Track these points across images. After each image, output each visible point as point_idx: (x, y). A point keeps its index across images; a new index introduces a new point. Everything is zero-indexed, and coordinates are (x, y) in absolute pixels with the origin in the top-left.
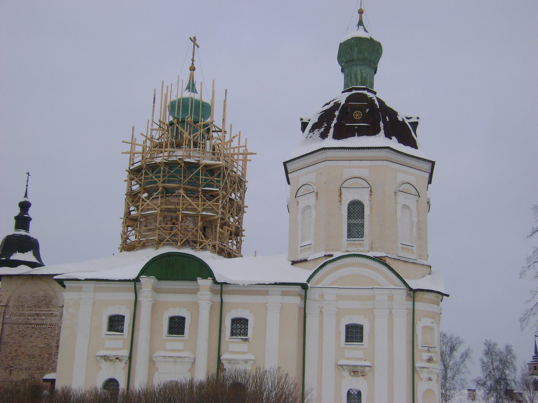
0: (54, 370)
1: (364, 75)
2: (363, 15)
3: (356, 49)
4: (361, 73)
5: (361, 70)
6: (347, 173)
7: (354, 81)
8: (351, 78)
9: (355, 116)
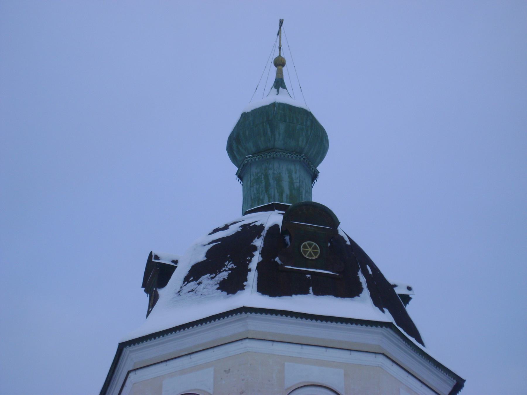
1: (297, 185)
2: (284, 69)
3: (282, 127)
4: (290, 177)
5: (290, 172)
7: (273, 191)
8: (267, 187)
9: (305, 252)
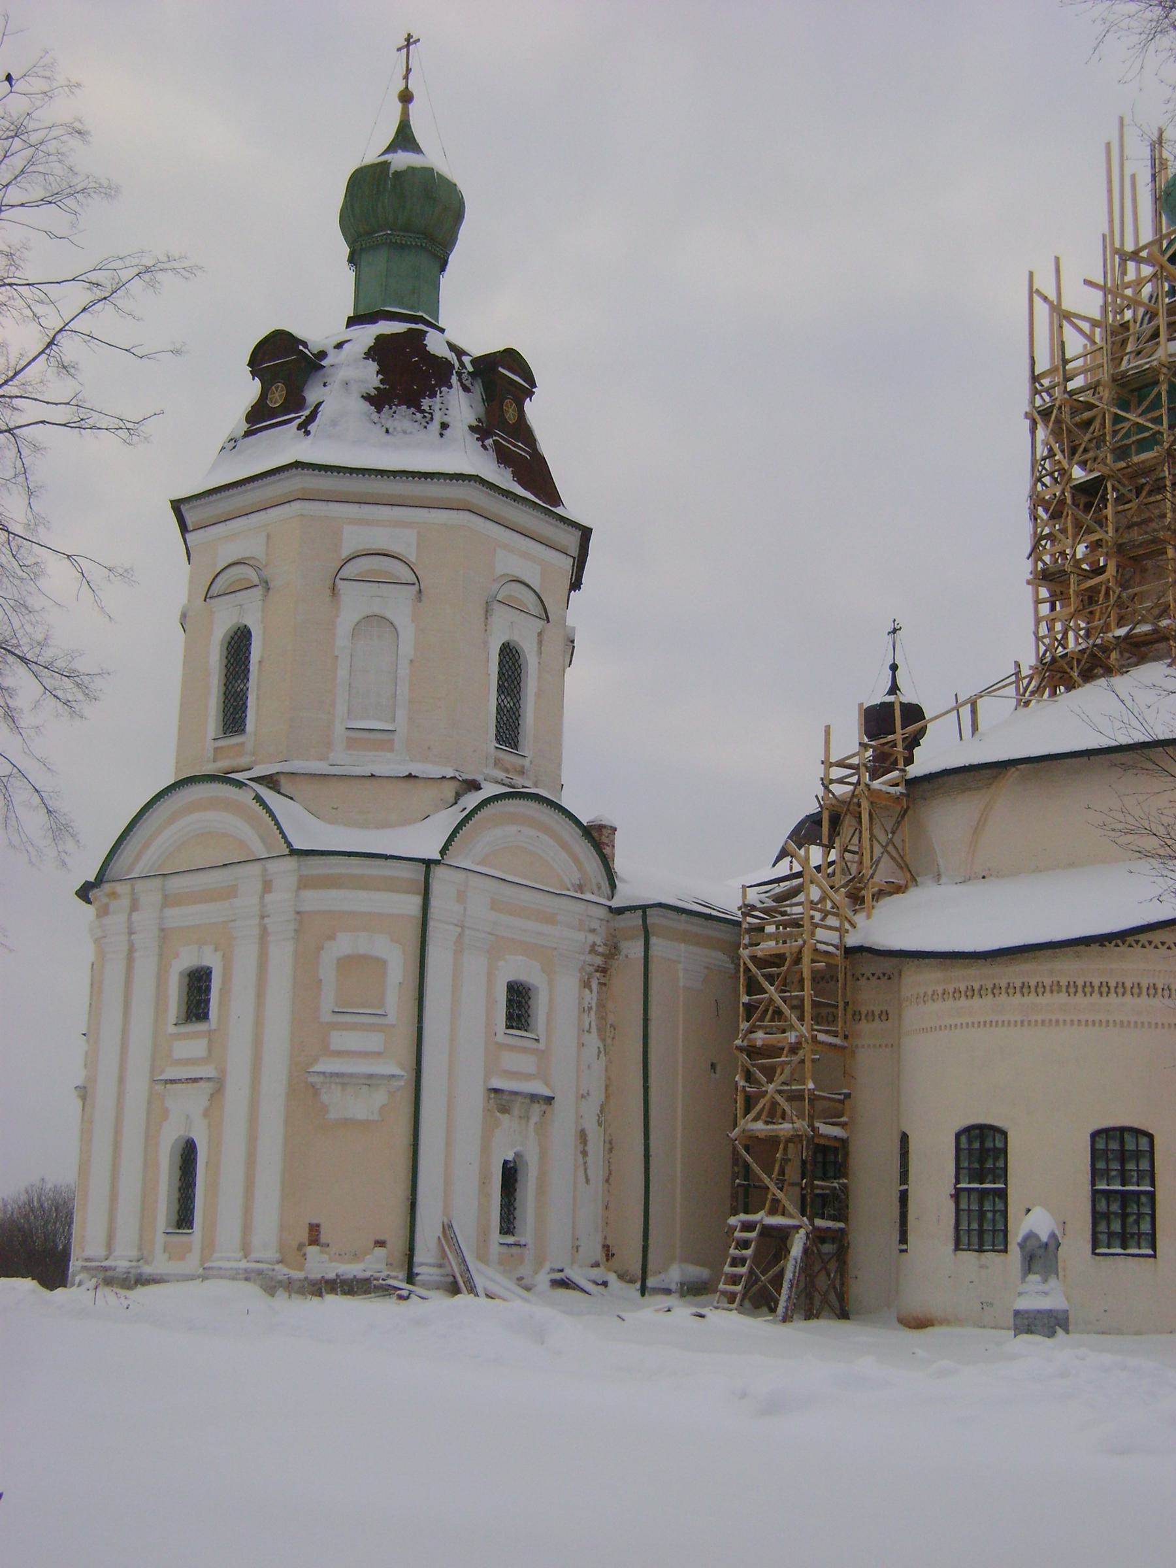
0: (846, 1176)
6: (354, 539)
